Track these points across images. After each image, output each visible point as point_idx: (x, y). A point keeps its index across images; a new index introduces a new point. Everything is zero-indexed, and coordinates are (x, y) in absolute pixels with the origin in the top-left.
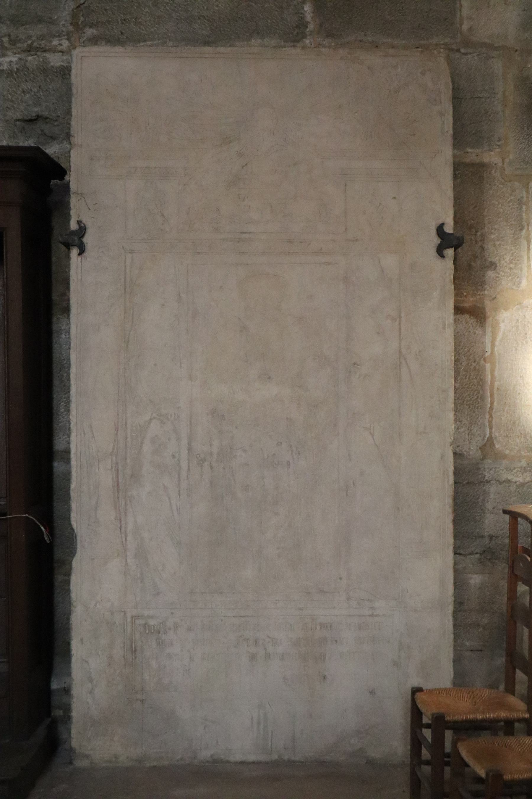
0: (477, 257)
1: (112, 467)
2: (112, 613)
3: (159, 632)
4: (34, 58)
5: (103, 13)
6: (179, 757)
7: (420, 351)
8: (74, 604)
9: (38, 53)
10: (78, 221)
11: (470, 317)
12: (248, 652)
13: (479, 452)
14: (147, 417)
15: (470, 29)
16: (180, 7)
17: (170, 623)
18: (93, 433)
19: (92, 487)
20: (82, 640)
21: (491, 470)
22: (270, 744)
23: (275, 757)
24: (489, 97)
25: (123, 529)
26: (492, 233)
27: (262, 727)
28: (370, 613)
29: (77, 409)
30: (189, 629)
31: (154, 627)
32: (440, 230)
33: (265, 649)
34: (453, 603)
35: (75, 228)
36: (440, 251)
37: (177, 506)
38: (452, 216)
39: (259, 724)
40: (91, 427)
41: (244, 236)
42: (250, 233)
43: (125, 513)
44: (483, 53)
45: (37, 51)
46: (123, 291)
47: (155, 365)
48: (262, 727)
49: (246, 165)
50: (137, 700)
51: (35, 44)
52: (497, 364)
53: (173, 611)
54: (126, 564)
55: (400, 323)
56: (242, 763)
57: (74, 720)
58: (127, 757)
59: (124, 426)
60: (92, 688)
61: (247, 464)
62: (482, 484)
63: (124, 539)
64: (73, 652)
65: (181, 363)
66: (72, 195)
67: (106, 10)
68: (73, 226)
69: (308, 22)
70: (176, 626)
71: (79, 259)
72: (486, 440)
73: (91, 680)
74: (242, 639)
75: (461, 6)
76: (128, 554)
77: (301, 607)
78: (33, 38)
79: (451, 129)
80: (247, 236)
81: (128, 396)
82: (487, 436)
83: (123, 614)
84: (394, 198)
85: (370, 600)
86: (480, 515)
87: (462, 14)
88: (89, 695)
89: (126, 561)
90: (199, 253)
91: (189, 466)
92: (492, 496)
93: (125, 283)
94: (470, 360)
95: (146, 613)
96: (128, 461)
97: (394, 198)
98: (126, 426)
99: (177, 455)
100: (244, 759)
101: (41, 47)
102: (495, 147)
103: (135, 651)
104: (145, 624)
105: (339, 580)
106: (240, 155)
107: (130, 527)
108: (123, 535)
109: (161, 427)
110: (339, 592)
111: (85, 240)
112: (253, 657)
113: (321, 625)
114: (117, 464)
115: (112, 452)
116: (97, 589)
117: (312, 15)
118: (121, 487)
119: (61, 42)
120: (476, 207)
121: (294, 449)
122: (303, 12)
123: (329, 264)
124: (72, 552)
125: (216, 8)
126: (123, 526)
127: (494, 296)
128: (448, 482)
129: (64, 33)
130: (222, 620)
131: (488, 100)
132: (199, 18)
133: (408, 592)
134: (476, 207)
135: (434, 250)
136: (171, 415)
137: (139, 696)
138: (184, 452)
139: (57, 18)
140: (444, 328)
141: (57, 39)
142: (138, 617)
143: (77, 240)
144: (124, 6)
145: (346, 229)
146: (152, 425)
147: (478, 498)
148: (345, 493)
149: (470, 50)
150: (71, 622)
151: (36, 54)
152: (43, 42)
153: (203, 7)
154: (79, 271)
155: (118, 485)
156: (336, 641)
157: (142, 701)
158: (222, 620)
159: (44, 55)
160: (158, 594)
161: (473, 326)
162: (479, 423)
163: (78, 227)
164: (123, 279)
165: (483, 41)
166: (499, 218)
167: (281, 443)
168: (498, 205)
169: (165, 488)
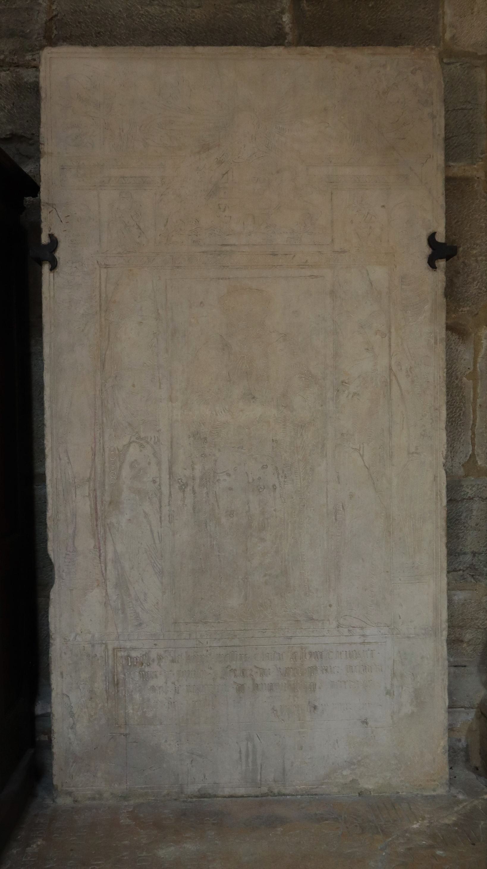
0: (459, 273)
1: (89, 494)
2: (93, 646)
3: (143, 664)
4: (8, 74)
5: (77, 26)
6: (165, 792)
7: (411, 368)
8: (53, 637)
9: (12, 69)
10: (49, 235)
11: (452, 334)
12: (235, 682)
13: (462, 469)
14: (126, 441)
15: (453, 38)
16: (156, 19)
17: (153, 655)
18: (69, 459)
19: (69, 515)
20: (62, 673)
21: (474, 486)
22: (259, 777)
23: (265, 790)
24: (471, 109)
25: (102, 558)
26: (474, 249)
27: (250, 760)
28: (361, 640)
29: (52, 434)
30: (173, 661)
31: (137, 659)
32: (431, 239)
33: (253, 680)
34: (447, 629)
35: (47, 242)
36: (432, 263)
37: (158, 533)
38: (444, 225)
39: (247, 756)
40: (66, 451)
41: (224, 248)
42: (231, 245)
43: (105, 542)
44: (467, 63)
45: (10, 66)
46: (98, 308)
47: (134, 386)
48: (250, 760)
49: (227, 173)
50: (121, 734)
51: (7, 60)
52: (480, 381)
53: (155, 642)
54: (107, 594)
55: (390, 338)
56: (231, 796)
57: (55, 757)
58: (112, 794)
59: (102, 451)
60: (74, 724)
61: (231, 489)
62: (465, 500)
63: (103, 568)
64: (54, 686)
65: (160, 383)
66: (42, 207)
67: (79, 23)
68: (45, 239)
69: (287, 34)
70: (160, 658)
71: (52, 274)
72: (468, 458)
73: (72, 715)
74: (229, 669)
75: (444, 13)
76: (108, 583)
77: (289, 635)
78: (6, 53)
79: (443, 132)
80: (228, 248)
81: (105, 419)
82: (470, 453)
83: (104, 646)
84: (383, 206)
85: (362, 628)
86: (463, 532)
87: (445, 21)
88: (70, 730)
89: (106, 590)
90: (178, 267)
91: (170, 492)
92: (475, 513)
93: (100, 300)
94: (452, 377)
95: (128, 645)
96: (107, 487)
97: (383, 206)
98: (104, 450)
99: (158, 480)
100: (232, 792)
101: (14, 62)
102: (478, 160)
103: (118, 684)
104: (128, 656)
105: (328, 607)
106: (220, 162)
107: (110, 555)
108: (103, 565)
109: (141, 451)
110: (329, 620)
111: (57, 254)
112: (241, 688)
113: (311, 654)
114: (95, 490)
115: (90, 478)
116: (78, 619)
117: (290, 25)
118: (99, 513)
119: (34, 57)
120: (458, 222)
121: (280, 472)
122: (281, 22)
123: (316, 277)
124: (49, 584)
125: (193, 20)
126: (103, 554)
127: (476, 313)
128: (441, 504)
129: (37, 48)
130: (207, 651)
131: (471, 112)
132: (175, 31)
133: (400, 618)
134: (458, 222)
135: (426, 261)
136: (151, 439)
137: (122, 731)
138: (165, 476)
139: (30, 32)
140: (436, 343)
141: (30, 53)
142: (120, 649)
143: (49, 254)
144: (98, 19)
145: (332, 240)
146: (131, 449)
147: (461, 516)
148: (334, 518)
149: (452, 60)
150: (50, 655)
151: (9, 70)
152: (16, 57)
153: (179, 19)
154: (52, 287)
155: (96, 512)
156: (326, 670)
157: (125, 735)
158: (207, 651)
159: (18, 70)
160: (140, 624)
161: (455, 343)
162: (462, 441)
163: (49, 241)
164: (98, 297)
165: (467, 50)
166: (481, 233)
167: (266, 465)
168: (481, 219)
169: (146, 515)
